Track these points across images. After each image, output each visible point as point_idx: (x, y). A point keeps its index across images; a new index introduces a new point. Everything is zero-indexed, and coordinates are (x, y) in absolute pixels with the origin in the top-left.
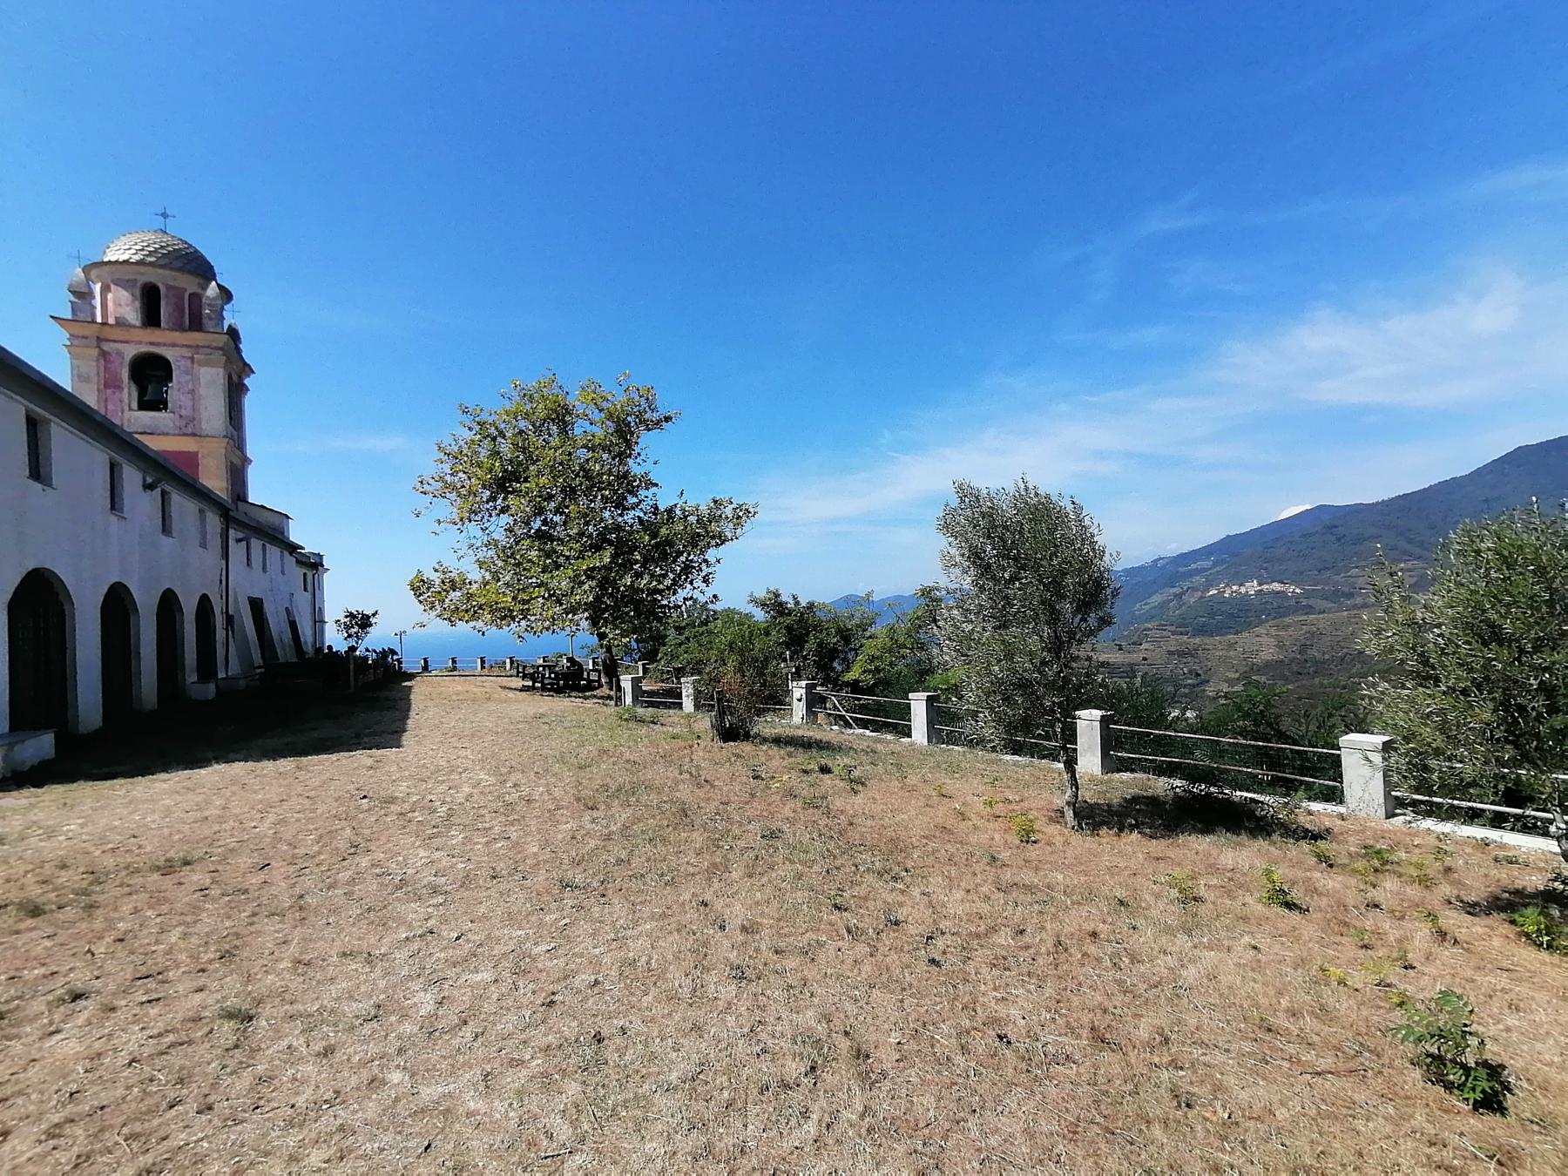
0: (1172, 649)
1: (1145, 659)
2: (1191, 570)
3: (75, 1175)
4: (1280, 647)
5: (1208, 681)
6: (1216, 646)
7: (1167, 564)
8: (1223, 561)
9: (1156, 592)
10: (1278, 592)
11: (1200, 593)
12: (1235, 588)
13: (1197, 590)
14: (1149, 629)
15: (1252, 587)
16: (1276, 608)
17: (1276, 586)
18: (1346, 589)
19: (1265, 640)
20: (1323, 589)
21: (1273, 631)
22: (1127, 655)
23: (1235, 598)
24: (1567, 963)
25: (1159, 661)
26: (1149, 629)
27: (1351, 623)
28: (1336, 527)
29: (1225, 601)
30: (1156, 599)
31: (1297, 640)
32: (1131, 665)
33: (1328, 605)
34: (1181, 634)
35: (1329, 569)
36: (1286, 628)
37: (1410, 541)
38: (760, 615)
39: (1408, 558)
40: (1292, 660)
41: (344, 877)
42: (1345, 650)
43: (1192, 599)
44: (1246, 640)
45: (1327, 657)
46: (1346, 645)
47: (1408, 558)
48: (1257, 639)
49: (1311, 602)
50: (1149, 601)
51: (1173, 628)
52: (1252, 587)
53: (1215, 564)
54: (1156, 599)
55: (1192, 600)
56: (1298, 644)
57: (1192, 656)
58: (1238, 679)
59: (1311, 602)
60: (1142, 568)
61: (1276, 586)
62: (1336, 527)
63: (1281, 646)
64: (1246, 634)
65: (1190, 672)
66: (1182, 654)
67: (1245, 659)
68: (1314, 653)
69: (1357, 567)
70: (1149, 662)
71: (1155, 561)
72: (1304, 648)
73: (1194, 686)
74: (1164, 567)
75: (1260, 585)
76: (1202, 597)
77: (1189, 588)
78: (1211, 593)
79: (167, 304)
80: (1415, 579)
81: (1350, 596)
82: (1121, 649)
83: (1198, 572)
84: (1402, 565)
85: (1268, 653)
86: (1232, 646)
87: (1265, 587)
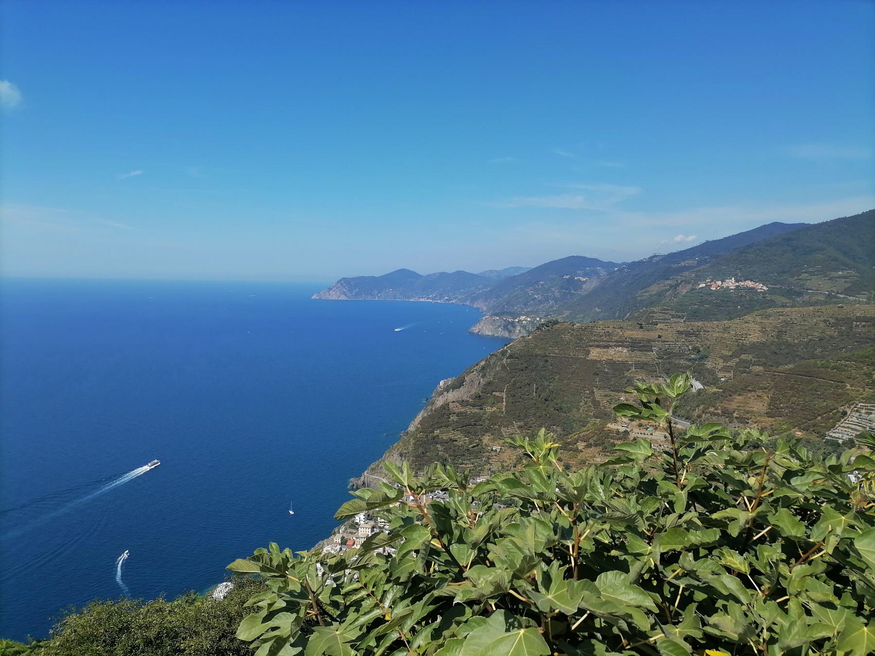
0: (681, 329)
1: (660, 337)
4: (763, 332)
7: (660, 260)
8: (705, 262)
11: (690, 285)
13: (689, 283)
15: (731, 283)
17: (749, 284)
18: (797, 289)
19: (752, 325)
20: (781, 288)
21: (758, 319)
22: (646, 333)
29: (711, 293)
30: (654, 289)
31: (775, 327)
32: (649, 341)
33: (785, 300)
38: (720, 648)
39: (844, 268)
40: (772, 343)
43: (684, 290)
45: (796, 341)
47: (844, 268)
49: (774, 297)
50: (648, 289)
52: (731, 283)
53: (700, 263)
54: (654, 289)
55: (685, 291)
56: (776, 330)
57: (696, 336)
58: (731, 356)
60: (641, 263)
61: (749, 284)
63: (763, 331)
64: (737, 321)
65: (694, 349)
66: (688, 334)
67: (737, 341)
68: (787, 338)
69: (806, 273)
70: (663, 339)
73: (695, 360)
75: (737, 281)
76: (693, 289)
77: (682, 281)
78: (700, 286)
79: (683, 499)
80: (850, 284)
81: (799, 294)
82: (641, 328)
83: (686, 268)
85: (755, 337)
86: (726, 329)
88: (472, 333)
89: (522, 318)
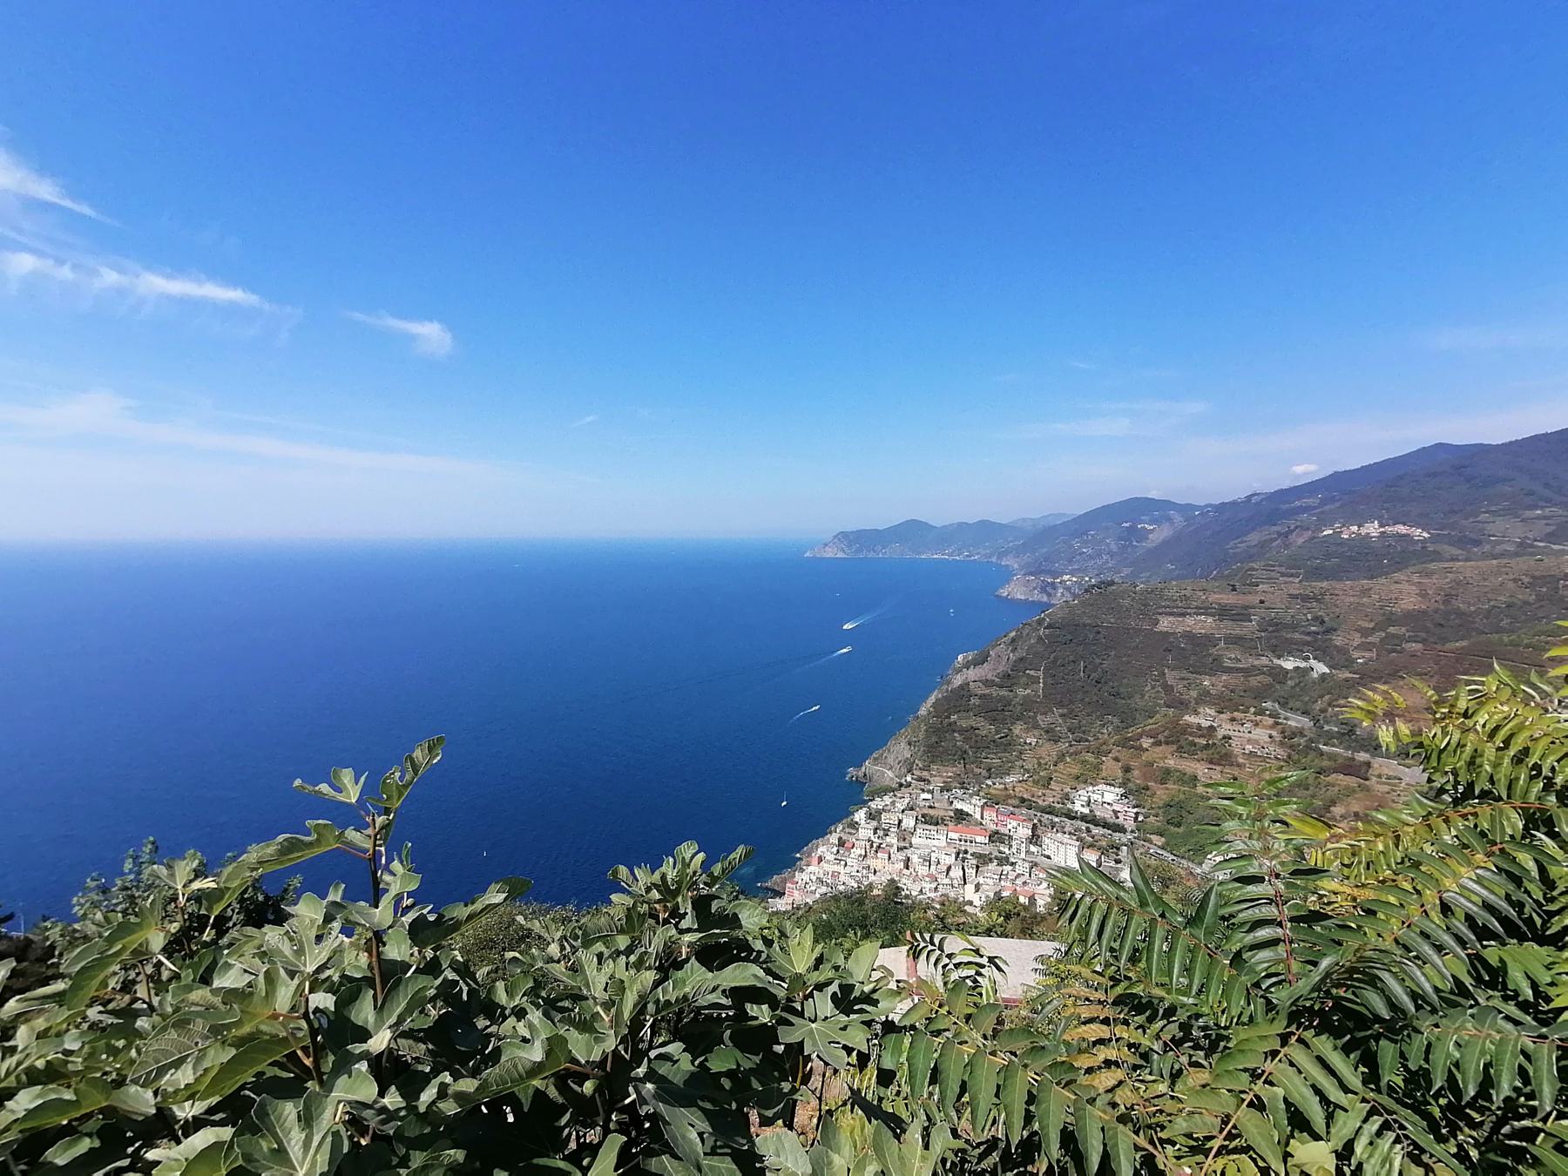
1: (1262, 602)
2: (1294, 508)
3: (423, 1175)
5: (1335, 630)
6: (1346, 592)
7: (1261, 501)
8: (1333, 500)
9: (1253, 529)
10: (1404, 535)
12: (1355, 528)
13: (1308, 529)
14: (1254, 570)
16: (1398, 556)
17: (1401, 529)
19: (1405, 587)
21: (1415, 578)
22: (1241, 596)
23: (1353, 539)
24: (1567, 866)
25: (1279, 605)
26: (1254, 570)
27: (1500, 575)
28: (1464, 467)
29: (1343, 543)
30: (1254, 538)
34: (1292, 576)
35: (1456, 513)
36: (1429, 574)
37: (1547, 485)
39: (1544, 504)
40: (1436, 611)
41: (1257, 1126)
42: (1492, 603)
44: (1381, 587)
45: (1472, 608)
46: (1494, 597)
48: (1398, 586)
49: (1439, 547)
51: (1283, 569)
52: (1373, 529)
53: (1323, 502)
54: (1254, 538)
55: (1300, 541)
57: (1318, 601)
58: (1373, 629)
59: (1439, 547)
60: (1234, 503)
61: (1401, 529)
62: (1464, 467)
63: (1423, 594)
65: (1315, 618)
66: (1305, 598)
71: (1249, 498)
72: (1448, 598)
74: (1258, 504)
75: (1381, 526)
77: (1296, 527)
78: (1325, 533)
81: (1478, 543)
82: (1234, 590)
84: (1538, 512)
86: (1366, 592)
87: (1389, 529)
88: (999, 597)
89: (1066, 577)
